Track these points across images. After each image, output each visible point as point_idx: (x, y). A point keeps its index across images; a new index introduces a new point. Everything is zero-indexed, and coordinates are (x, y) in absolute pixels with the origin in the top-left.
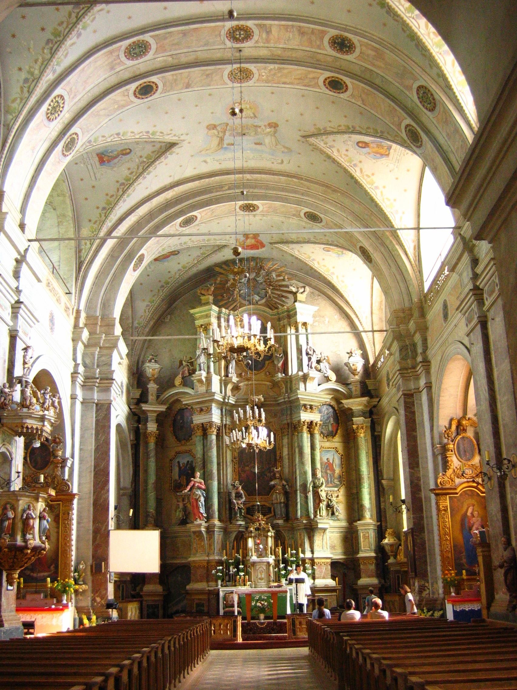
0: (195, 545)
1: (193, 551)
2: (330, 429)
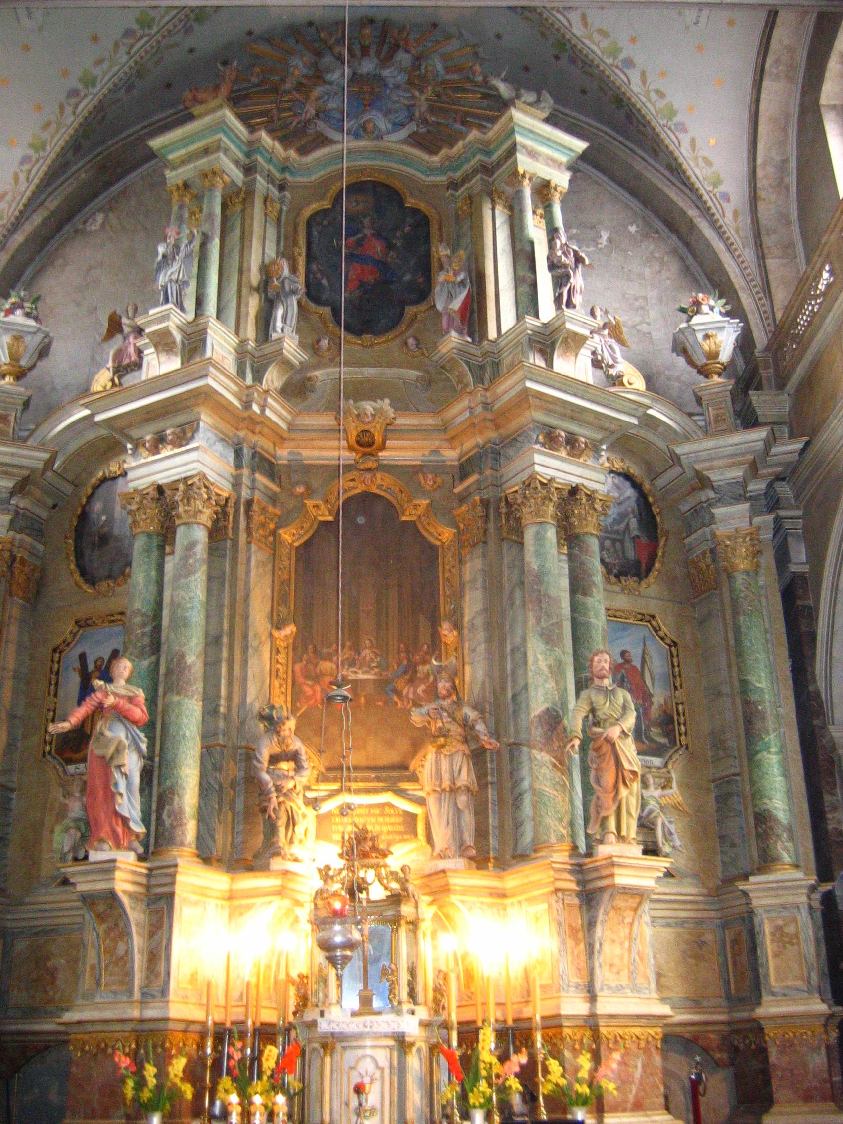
0: (91, 957)
1: (87, 982)
2: (631, 553)
